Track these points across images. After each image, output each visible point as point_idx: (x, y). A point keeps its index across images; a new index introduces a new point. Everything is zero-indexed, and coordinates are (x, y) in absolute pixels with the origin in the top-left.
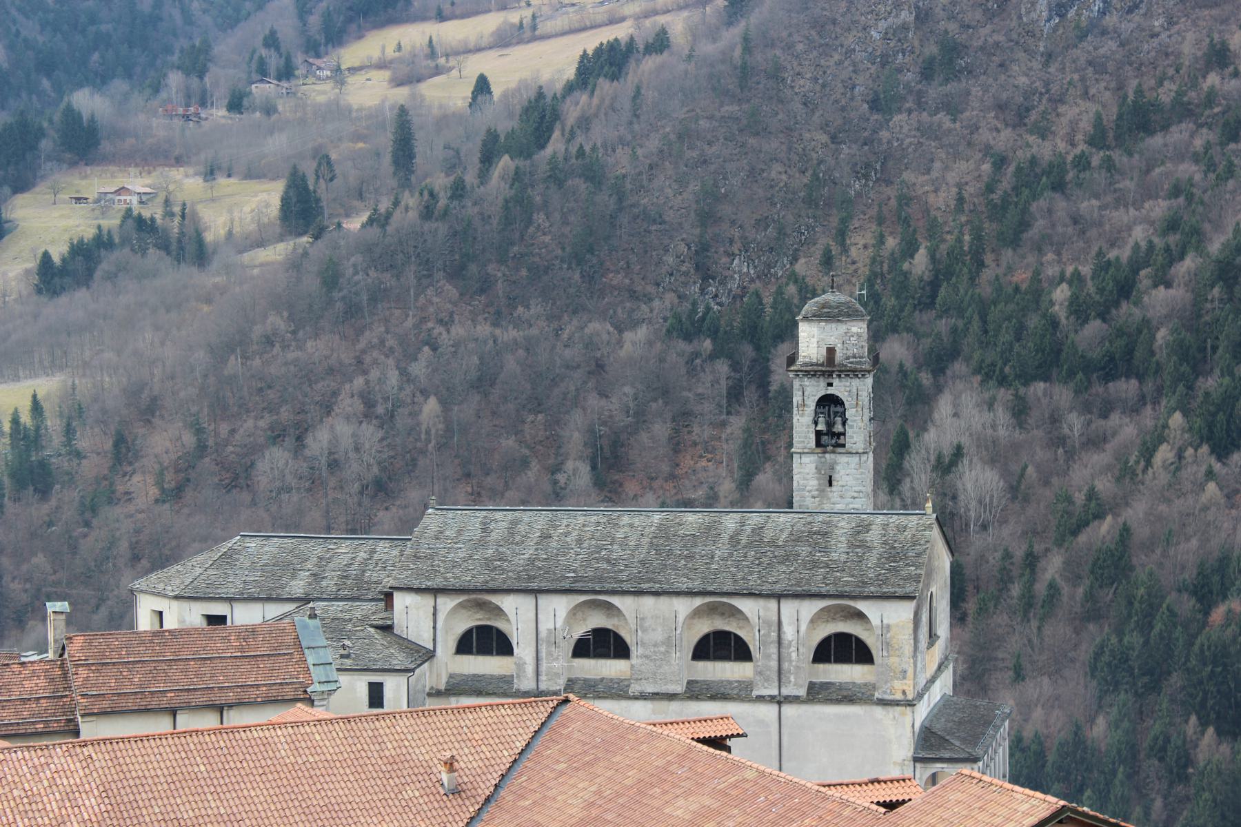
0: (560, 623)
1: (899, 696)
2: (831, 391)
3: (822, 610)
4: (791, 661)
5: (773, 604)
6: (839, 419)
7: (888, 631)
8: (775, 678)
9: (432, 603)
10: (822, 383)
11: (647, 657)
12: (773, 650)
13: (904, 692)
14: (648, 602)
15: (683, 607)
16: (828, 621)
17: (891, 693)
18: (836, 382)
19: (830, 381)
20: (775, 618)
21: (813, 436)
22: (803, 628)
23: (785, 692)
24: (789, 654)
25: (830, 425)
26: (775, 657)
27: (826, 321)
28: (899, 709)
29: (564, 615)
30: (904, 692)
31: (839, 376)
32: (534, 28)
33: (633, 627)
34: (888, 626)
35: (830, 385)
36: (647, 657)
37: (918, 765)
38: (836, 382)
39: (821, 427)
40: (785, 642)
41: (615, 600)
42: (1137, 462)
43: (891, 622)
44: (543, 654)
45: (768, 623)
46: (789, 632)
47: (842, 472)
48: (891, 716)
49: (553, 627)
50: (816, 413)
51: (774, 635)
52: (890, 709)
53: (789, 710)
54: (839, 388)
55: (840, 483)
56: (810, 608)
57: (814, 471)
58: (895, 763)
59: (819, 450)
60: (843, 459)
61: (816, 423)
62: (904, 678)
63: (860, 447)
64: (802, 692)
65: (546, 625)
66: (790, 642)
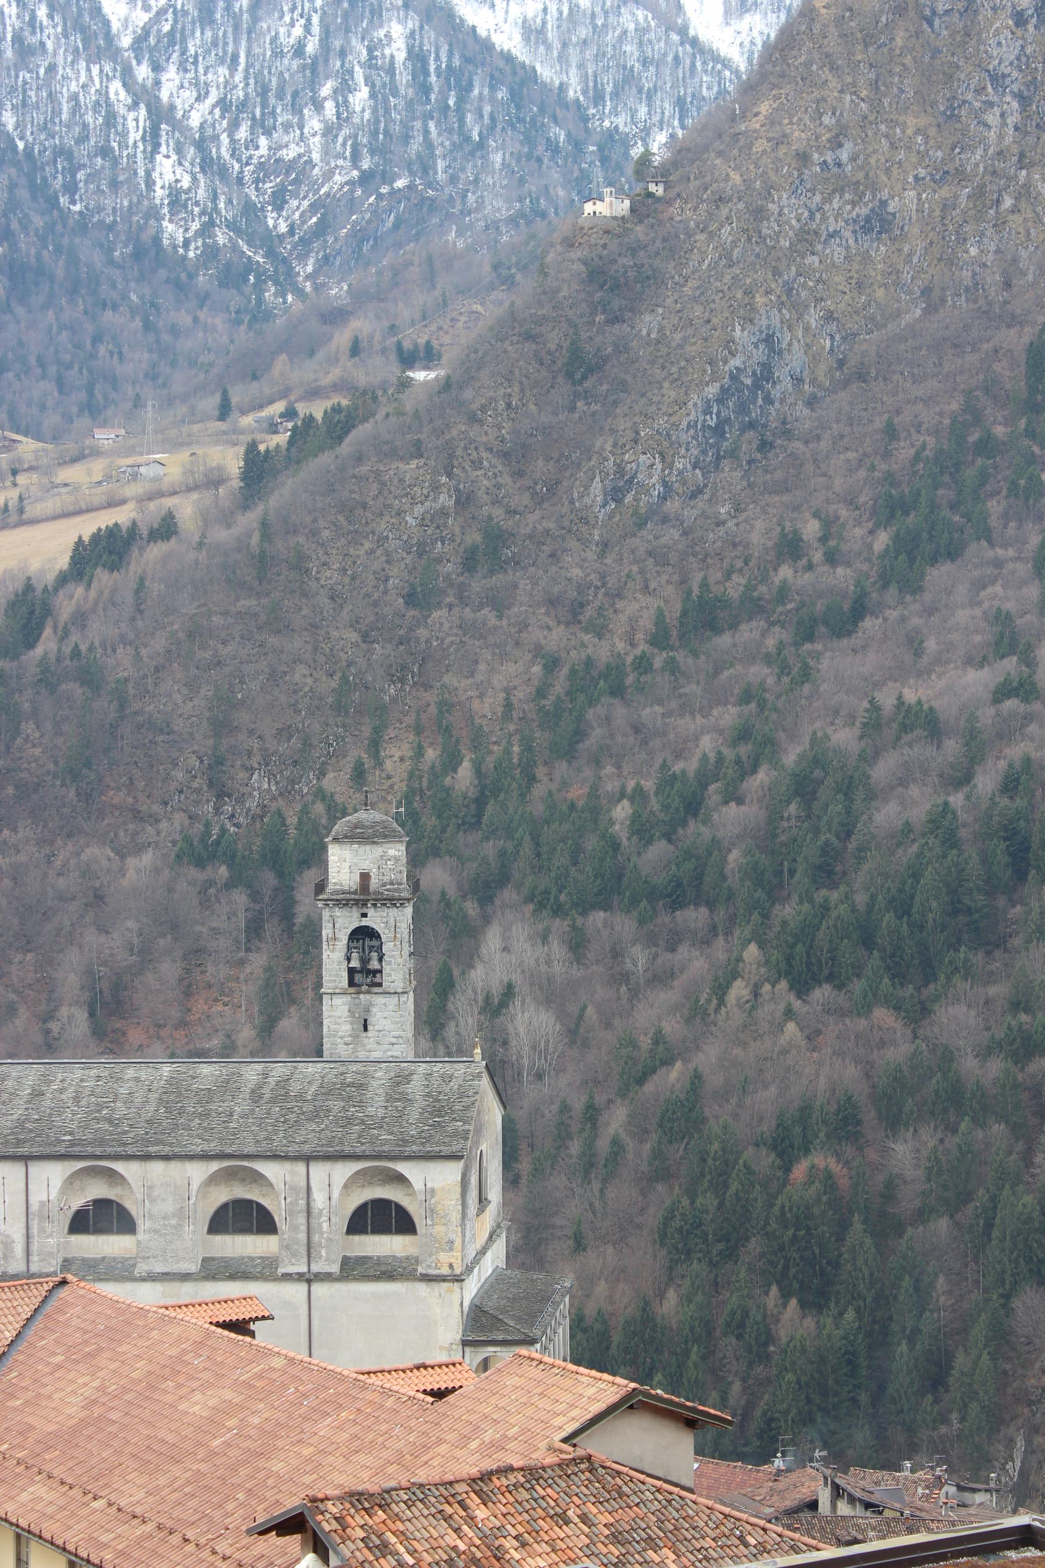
0: (54, 1194)
1: (445, 1271)
2: (365, 922)
3: (358, 1173)
4: (321, 1233)
5: (300, 1168)
6: (375, 955)
7: (433, 1196)
8: (304, 1253)
9: (304, 1169)
10: (356, 913)
11: (156, 1231)
12: (302, 1220)
13: (451, 1266)
14: (157, 1169)
15: (198, 1172)
16: (363, 1186)
17: (437, 1268)
18: (371, 912)
19: (365, 911)
20: (304, 1183)
21: (345, 975)
22: (336, 1195)
23: (315, 1268)
24: (320, 1225)
25: (364, 961)
26: (304, 1228)
27: (359, 843)
28: (445, 1285)
29: (60, 1184)
30: (451, 1266)
31: (375, 905)
32: (21, 511)
33: (140, 1197)
34: (433, 1190)
35: (364, 915)
36: (156, 1231)
37: (467, 1349)
38: (371, 912)
39: (355, 963)
40: (315, 1211)
41: (119, 1167)
42: (709, 1001)
43: (436, 1185)
44: (35, 1230)
45: (295, 1189)
46: (319, 1199)
47: (379, 1015)
48: (436, 1293)
49: (45, 1199)
50: (349, 948)
51: (302, 1203)
52: (435, 1285)
53: (319, 1290)
54: (375, 919)
55: (377, 1028)
56: (343, 1171)
57: (347, 1014)
58: (441, 1348)
59: (352, 990)
60: (380, 1000)
61: (349, 959)
62: (451, 1249)
63: (399, 986)
64: (335, 1268)
65: (38, 1196)
66: (321, 1211)
